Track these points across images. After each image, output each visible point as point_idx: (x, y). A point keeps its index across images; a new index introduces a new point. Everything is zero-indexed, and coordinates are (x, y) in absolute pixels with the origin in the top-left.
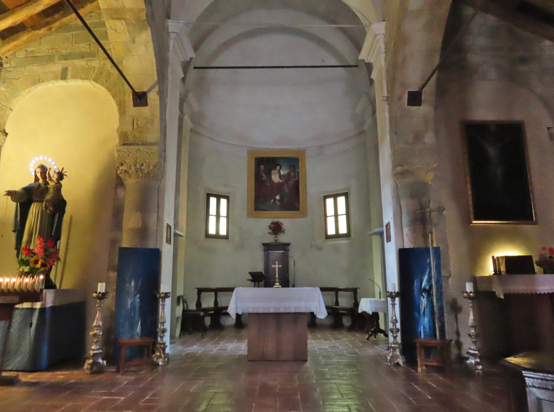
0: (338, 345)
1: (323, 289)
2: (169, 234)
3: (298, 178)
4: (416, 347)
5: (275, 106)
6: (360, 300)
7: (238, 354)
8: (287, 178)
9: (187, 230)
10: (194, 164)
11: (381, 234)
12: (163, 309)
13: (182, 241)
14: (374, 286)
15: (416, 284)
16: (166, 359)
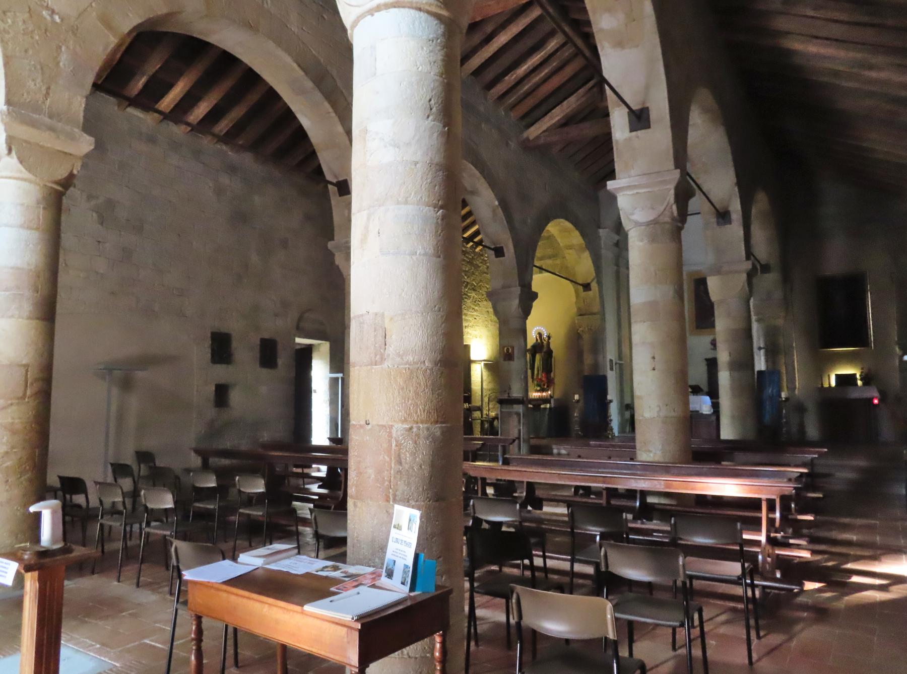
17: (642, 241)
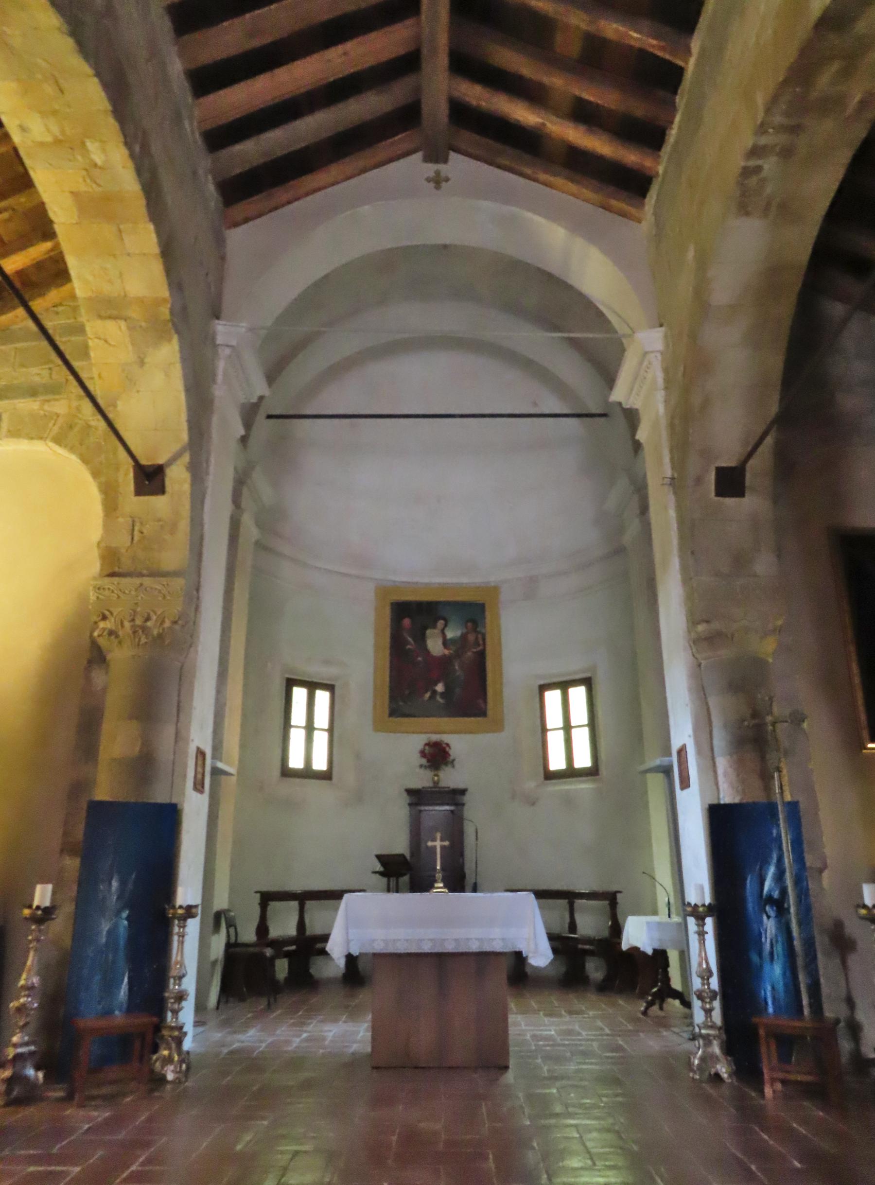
0: (577, 1028)
1: (541, 895)
2: (200, 769)
3: (484, 644)
4: (756, 1034)
5: (437, 492)
6: (625, 921)
7: (351, 1050)
8: (462, 643)
9: (241, 761)
10: (259, 608)
11: (667, 771)
12: (181, 943)
13: (230, 785)
14: (655, 886)
15: (750, 884)
16: (184, 1066)
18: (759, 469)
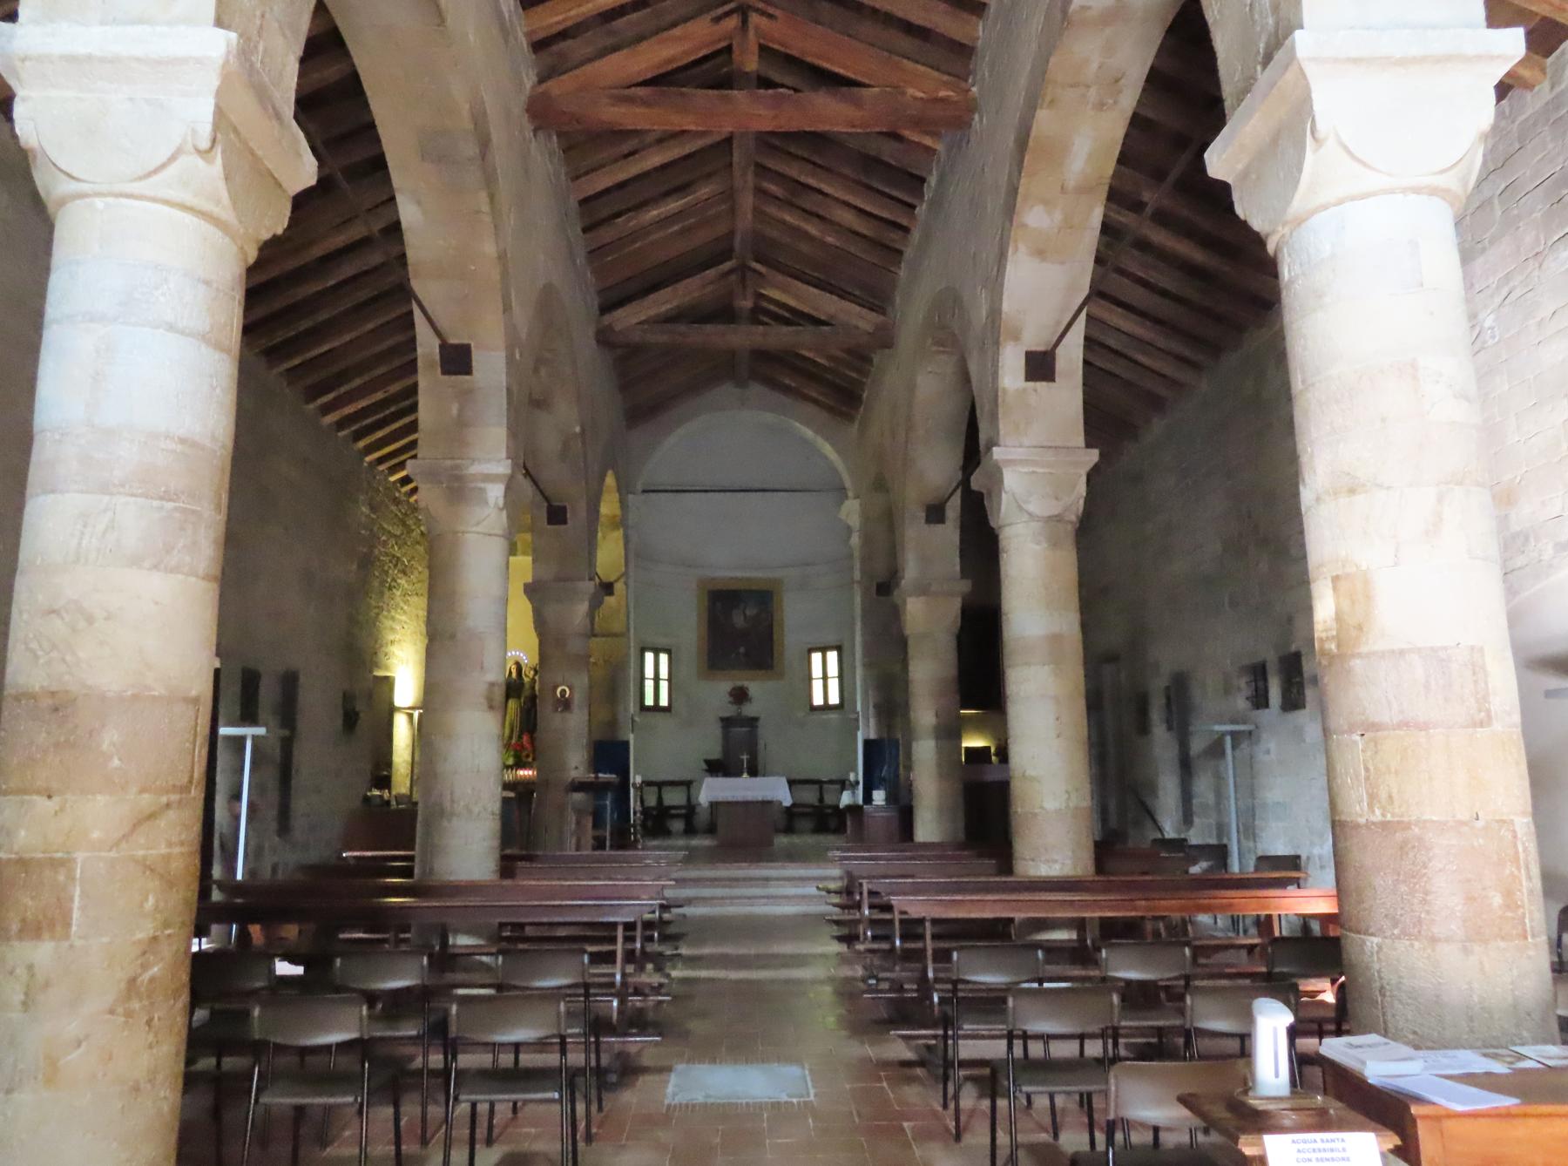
17: (1038, 543)
18: (1071, 355)
